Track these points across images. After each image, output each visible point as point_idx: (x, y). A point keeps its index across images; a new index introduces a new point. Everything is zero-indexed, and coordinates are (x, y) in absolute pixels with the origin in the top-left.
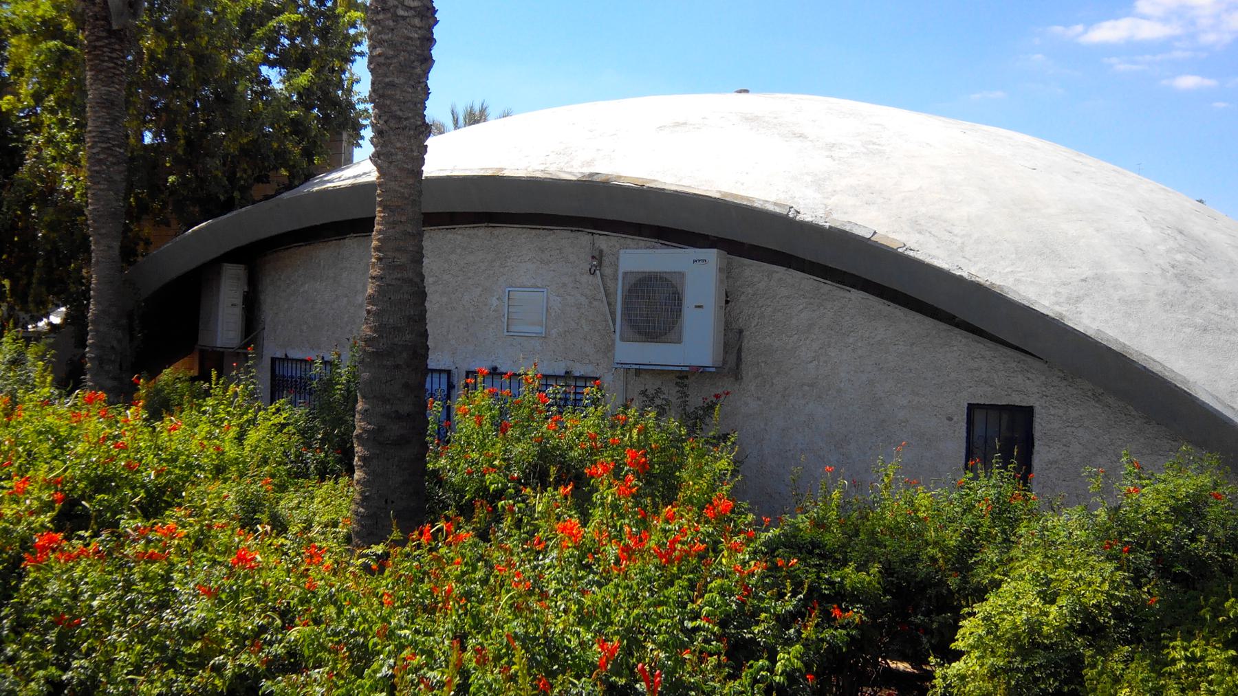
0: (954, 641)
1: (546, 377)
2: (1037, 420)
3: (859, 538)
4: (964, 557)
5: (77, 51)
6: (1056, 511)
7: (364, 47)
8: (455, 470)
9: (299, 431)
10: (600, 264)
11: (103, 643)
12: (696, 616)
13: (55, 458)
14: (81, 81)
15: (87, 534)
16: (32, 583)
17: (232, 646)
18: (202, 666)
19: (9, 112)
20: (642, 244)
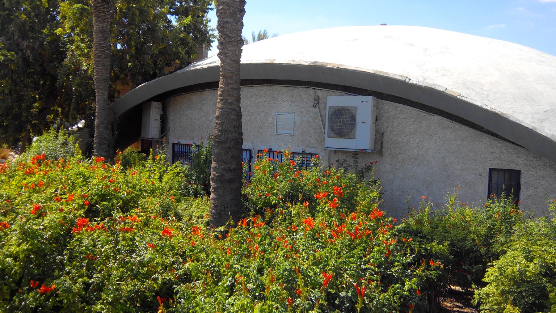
1: (293, 153)
2: (522, 176)
3: (438, 228)
4: (488, 240)
5: (89, 8)
6: (532, 219)
8: (253, 194)
9: (185, 176)
10: (318, 103)
11: (106, 267)
12: (366, 263)
13: (84, 185)
14: (90, 21)
15: (99, 219)
16: (77, 240)
17: (161, 270)
18: (148, 278)
19: (60, 36)
20: (337, 94)
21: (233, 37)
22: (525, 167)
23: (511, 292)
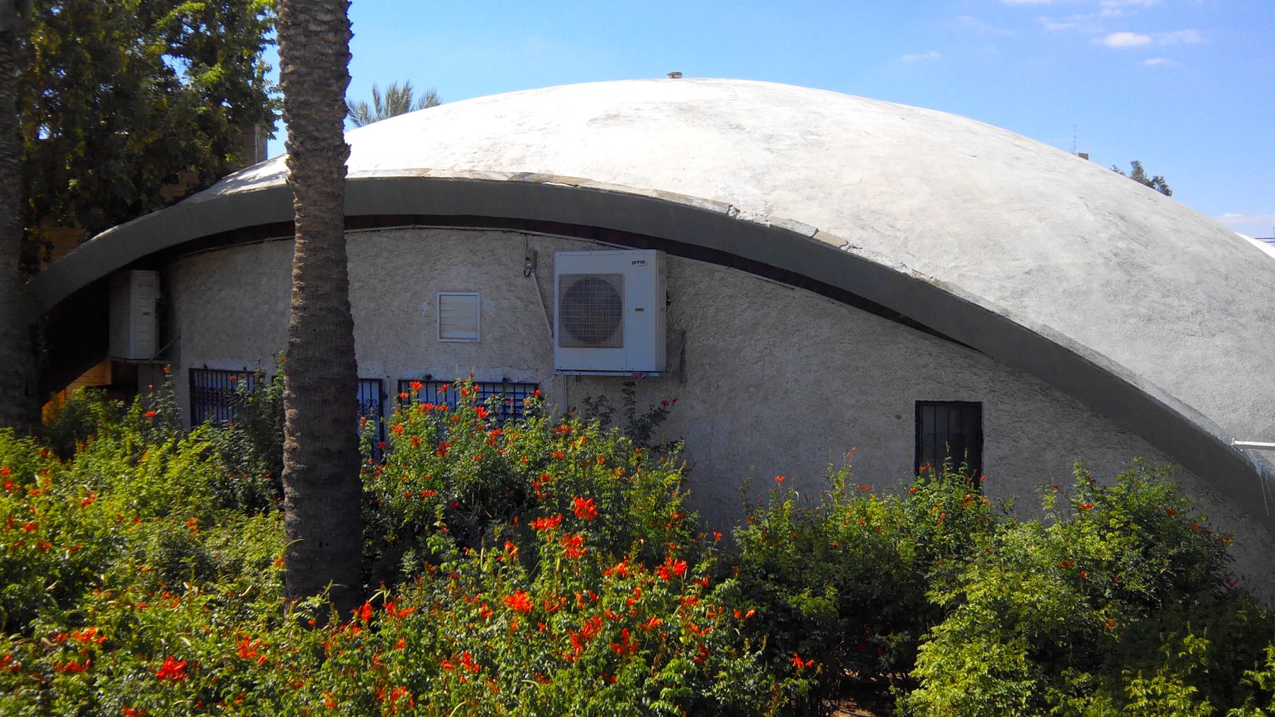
0: (914, 668)
1: (483, 384)
7: (273, 35)
10: (535, 265)
12: (654, 695)
20: (578, 244)
21: (324, 139)
22: (990, 396)
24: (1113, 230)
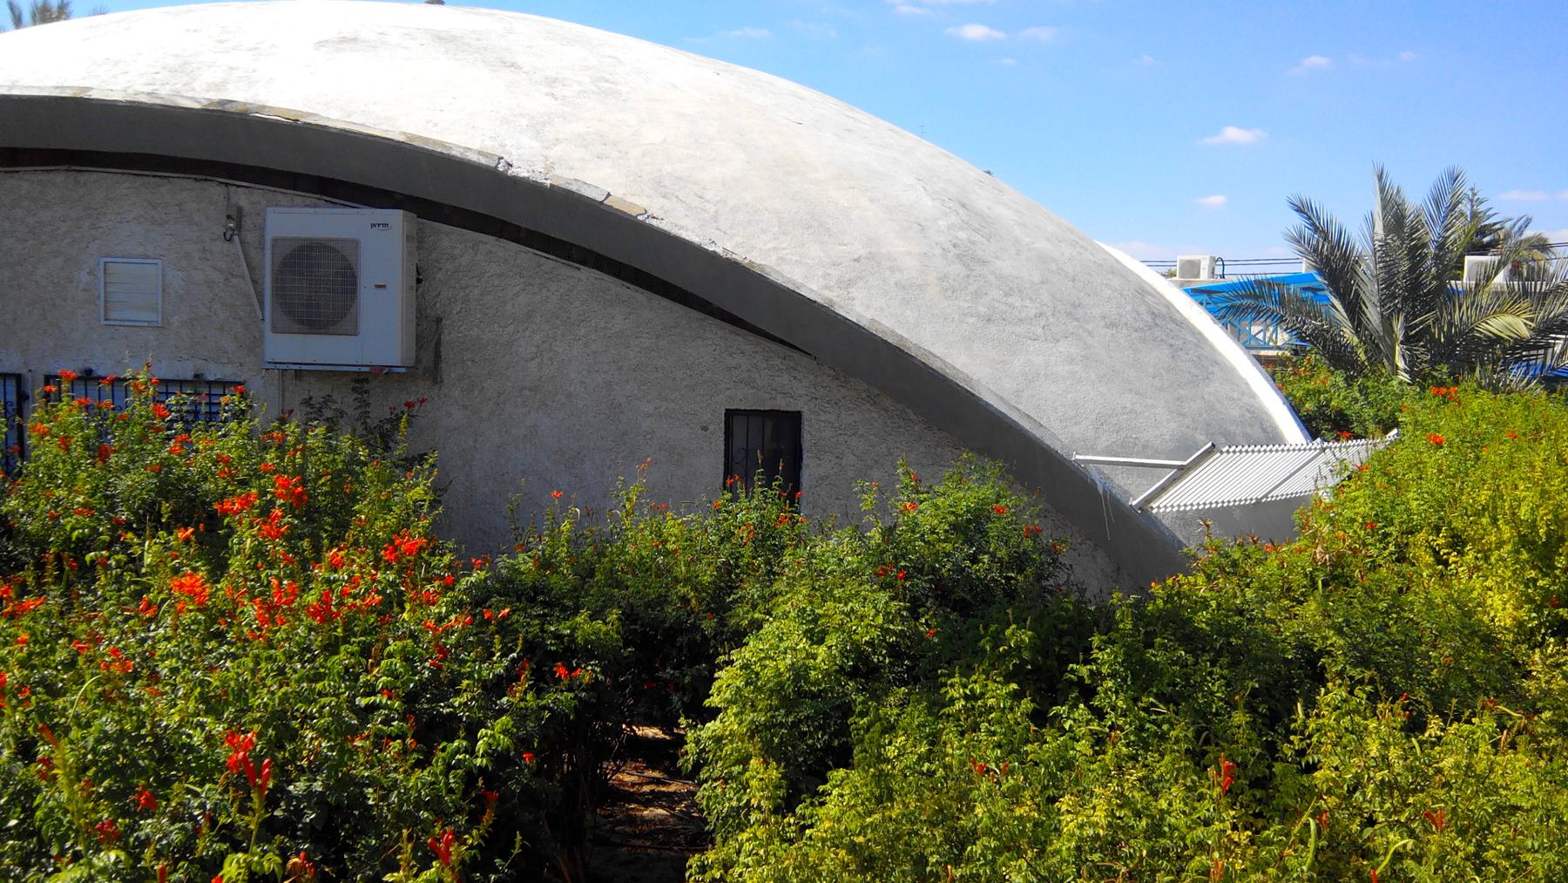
0: (709, 696)
1: (165, 382)
3: (592, 577)
10: (239, 227)
20: (298, 200)
23: (774, 726)
24: (953, 218)
